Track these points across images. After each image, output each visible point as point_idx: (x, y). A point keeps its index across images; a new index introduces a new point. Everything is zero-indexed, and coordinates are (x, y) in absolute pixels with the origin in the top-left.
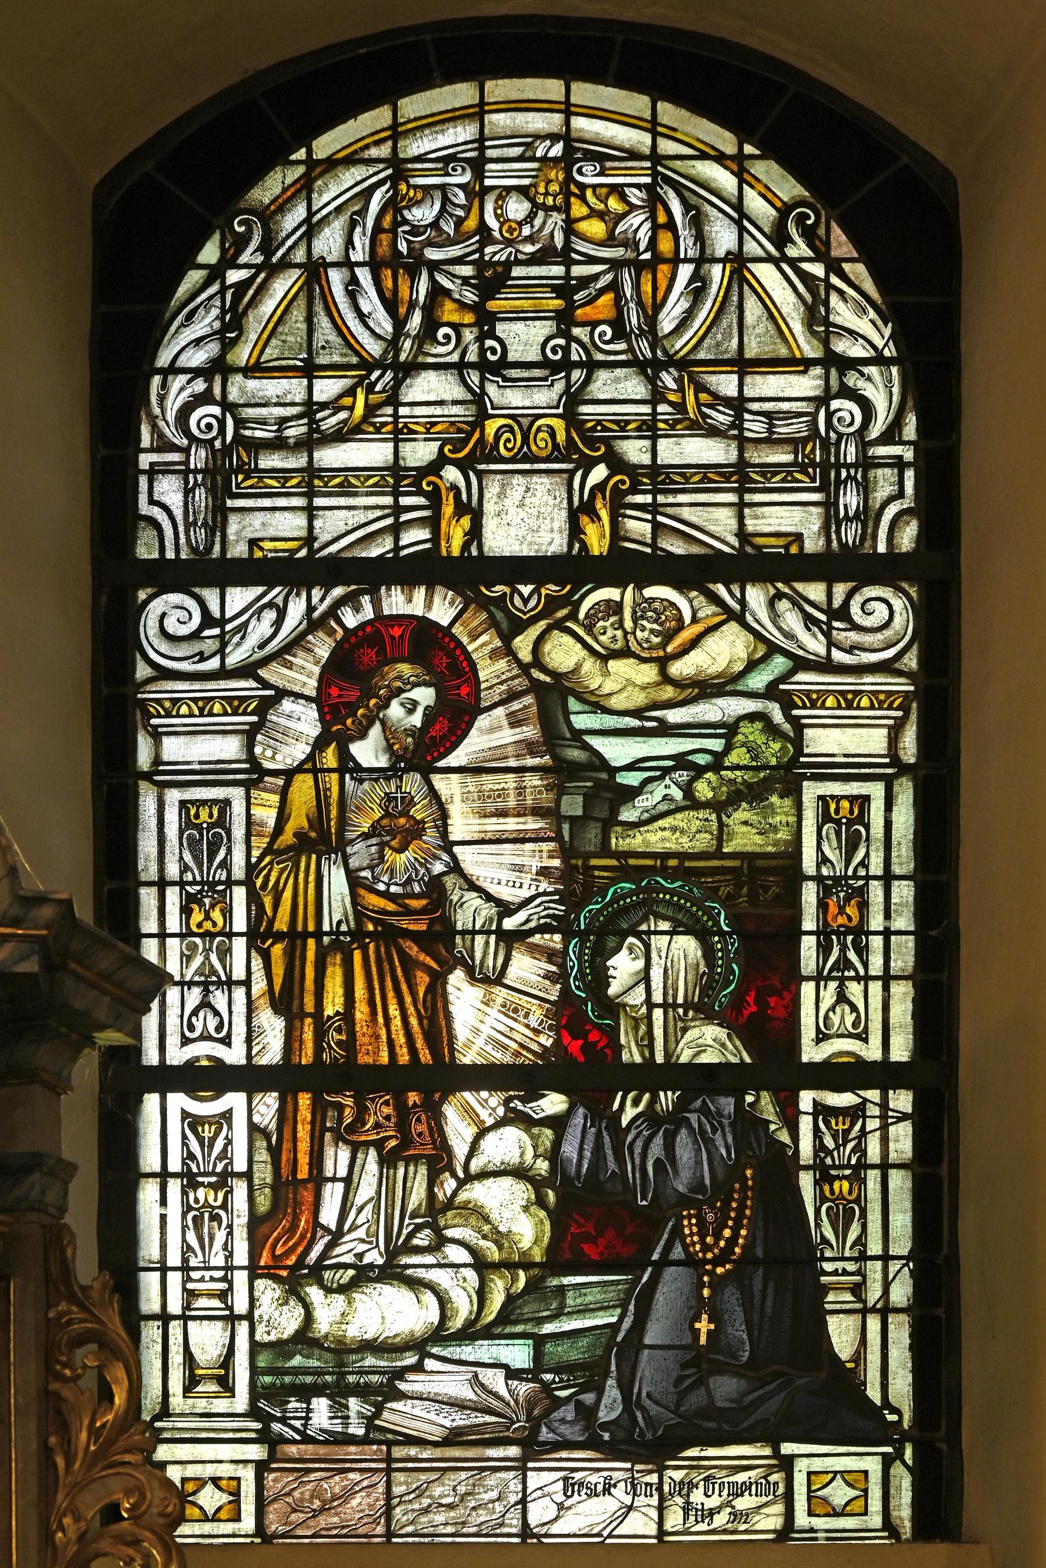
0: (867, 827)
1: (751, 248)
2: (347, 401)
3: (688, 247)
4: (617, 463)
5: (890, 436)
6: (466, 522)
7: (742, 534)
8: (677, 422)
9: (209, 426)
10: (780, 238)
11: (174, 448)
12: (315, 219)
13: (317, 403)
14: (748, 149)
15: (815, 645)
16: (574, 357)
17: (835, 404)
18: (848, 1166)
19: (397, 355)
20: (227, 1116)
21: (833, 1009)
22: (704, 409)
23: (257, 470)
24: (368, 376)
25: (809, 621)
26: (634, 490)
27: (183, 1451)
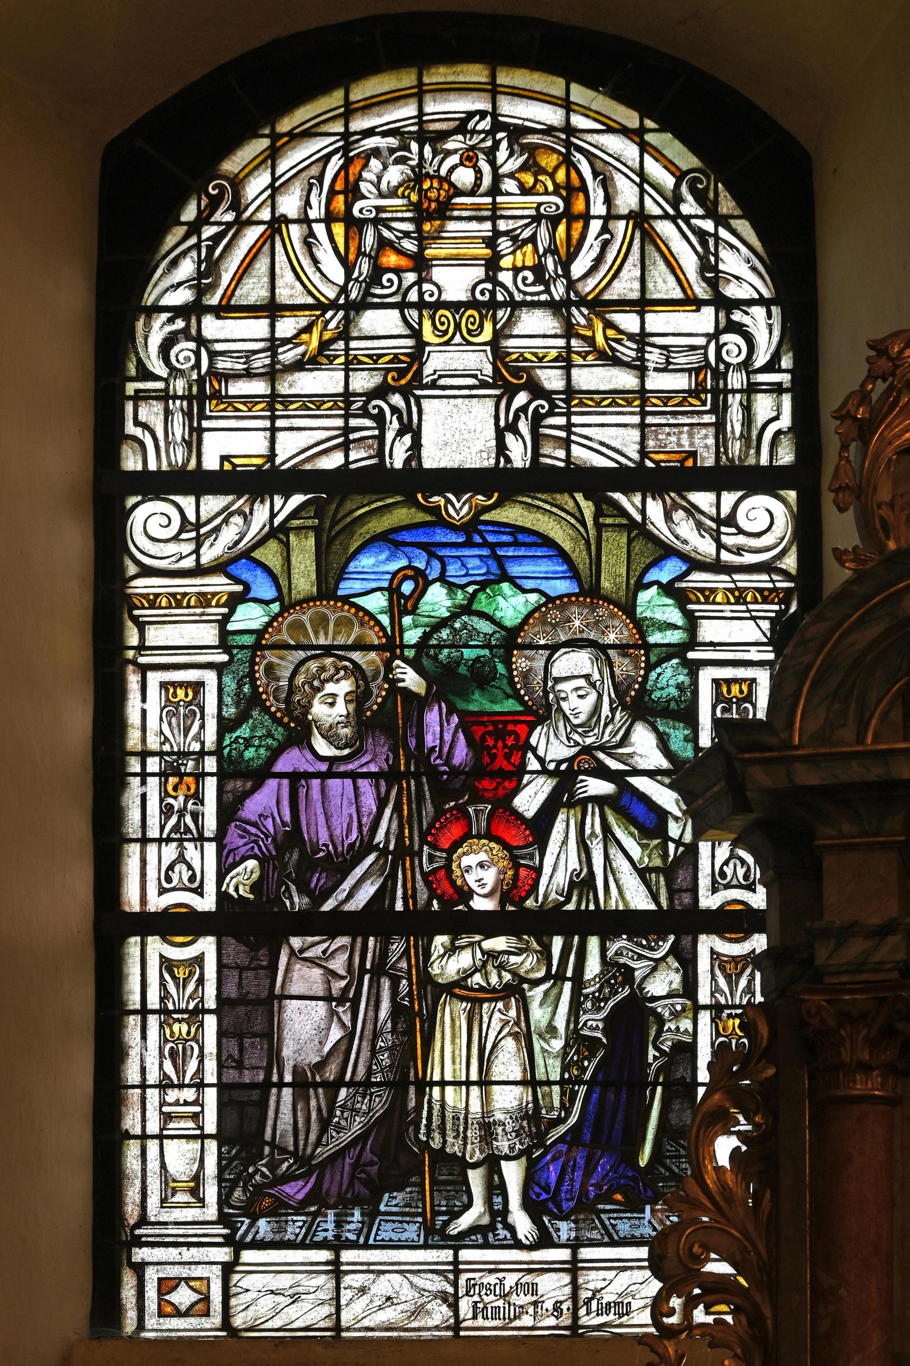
0: (754, 706)
1: (652, 208)
2: (305, 337)
3: (598, 208)
4: (537, 390)
5: (772, 366)
6: (407, 439)
7: (643, 452)
8: (588, 353)
9: (188, 359)
10: (676, 200)
11: (157, 378)
12: (277, 184)
13: (278, 339)
14: (649, 124)
15: (706, 547)
16: (500, 298)
17: (725, 338)
18: (740, 1006)
19: (347, 297)
20: (199, 960)
21: (726, 863)
22: (613, 344)
23: (227, 396)
24: (323, 315)
25: (699, 525)
26: (551, 413)
27: (159, 1254)
